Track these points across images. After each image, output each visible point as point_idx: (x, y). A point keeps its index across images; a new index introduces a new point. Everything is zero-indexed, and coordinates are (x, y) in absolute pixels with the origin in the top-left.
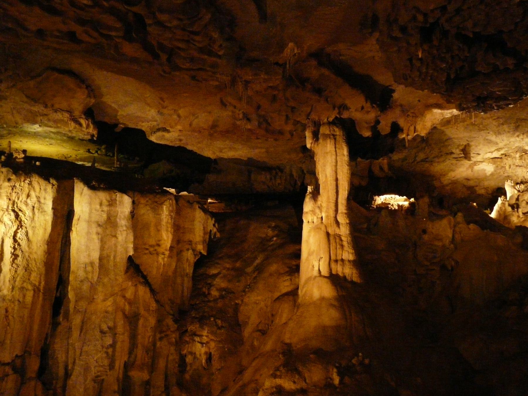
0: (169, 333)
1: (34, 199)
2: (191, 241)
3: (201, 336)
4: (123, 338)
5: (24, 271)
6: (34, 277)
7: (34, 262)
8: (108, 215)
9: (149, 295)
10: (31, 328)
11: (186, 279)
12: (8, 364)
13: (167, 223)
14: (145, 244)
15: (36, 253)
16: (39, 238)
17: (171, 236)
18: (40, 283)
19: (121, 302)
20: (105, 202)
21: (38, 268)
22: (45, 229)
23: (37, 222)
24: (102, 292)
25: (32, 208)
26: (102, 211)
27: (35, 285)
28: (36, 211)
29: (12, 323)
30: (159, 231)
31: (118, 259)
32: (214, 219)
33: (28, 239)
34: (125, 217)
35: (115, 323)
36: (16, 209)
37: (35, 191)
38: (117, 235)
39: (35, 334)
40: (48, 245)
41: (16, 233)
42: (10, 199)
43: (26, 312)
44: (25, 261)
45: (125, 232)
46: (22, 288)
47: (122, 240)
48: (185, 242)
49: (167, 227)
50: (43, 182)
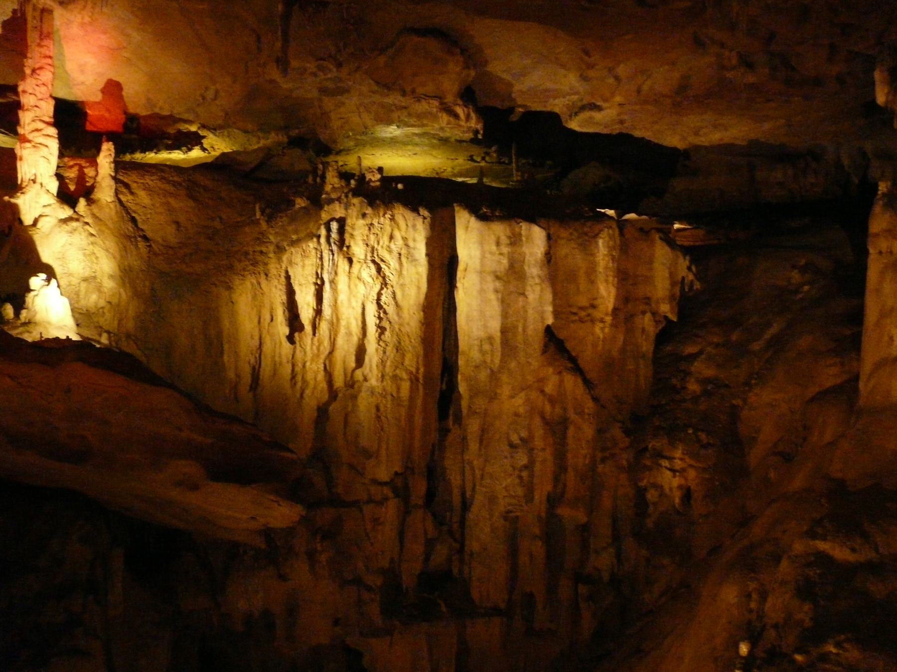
1: (400, 242)
3: (671, 459)
4: (545, 457)
5: (395, 351)
6: (409, 361)
12: (386, 484)
13: (606, 268)
16: (412, 302)
17: (613, 291)
18: (418, 369)
20: (504, 240)
21: (414, 347)
22: (419, 288)
26: (501, 254)
27: (411, 373)
28: (404, 260)
30: (592, 282)
32: (688, 258)
33: (397, 304)
34: (536, 261)
35: (530, 430)
36: (377, 260)
37: (399, 229)
38: (527, 293)
39: (417, 444)
40: (424, 311)
41: (379, 294)
42: (367, 245)
46: (395, 378)
50: (410, 215)
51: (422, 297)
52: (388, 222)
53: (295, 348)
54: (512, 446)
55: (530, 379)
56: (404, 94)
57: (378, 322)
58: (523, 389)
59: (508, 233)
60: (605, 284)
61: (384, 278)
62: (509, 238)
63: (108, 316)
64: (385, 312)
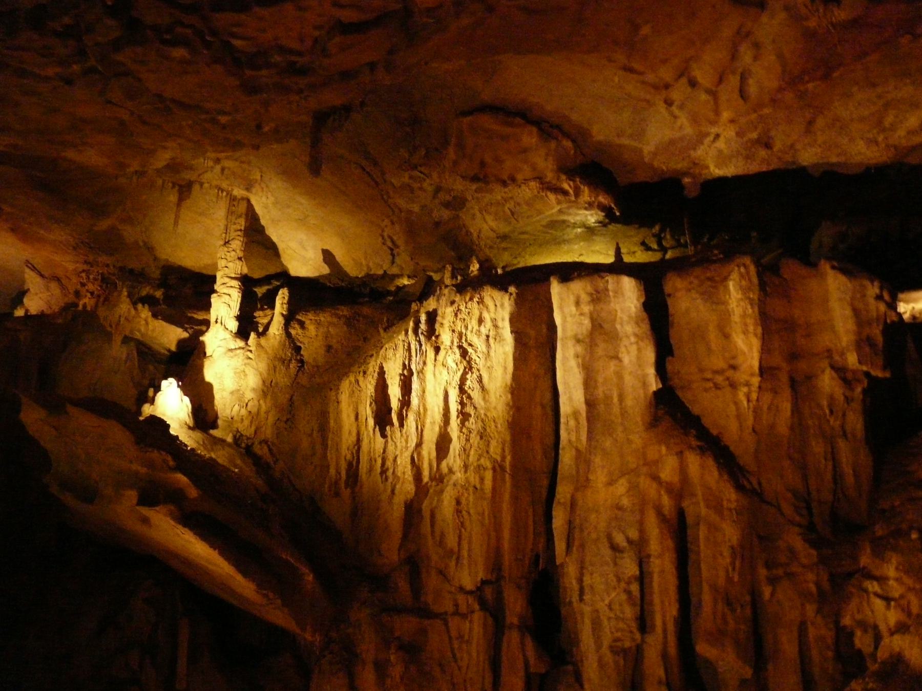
0: (795, 568)
1: (488, 324)
2: (829, 351)
3: (882, 580)
4: (662, 566)
5: (478, 437)
6: (495, 448)
7: (493, 424)
8: (592, 320)
9: (716, 473)
10: (499, 539)
11: (842, 444)
12: (470, 592)
13: (744, 316)
14: (701, 370)
15: (495, 408)
16: (498, 384)
17: (756, 343)
18: (503, 458)
19: (651, 489)
20: (585, 298)
21: (499, 433)
22: (505, 368)
23: (494, 360)
24: (603, 467)
25: (484, 337)
26: (581, 314)
27: (495, 461)
28: (491, 341)
29: (467, 524)
30: (727, 336)
31: (629, 402)
32: (876, 283)
33: (483, 388)
34: (630, 317)
35: (642, 531)
36: (465, 345)
37: (489, 312)
38: (620, 355)
39: (506, 545)
40: (512, 393)
41: (463, 380)
42: (453, 331)
43: (485, 505)
44: (479, 421)
45: (634, 347)
46: (480, 468)
47: (630, 361)
48: (818, 355)
49: (746, 325)
50: (497, 294)
51: (509, 377)
52: (475, 305)
53: (386, 442)
54: (614, 548)
55: (632, 462)
56: (504, 184)
57: (460, 407)
58: (623, 475)
59: (589, 289)
60: (742, 336)
61: (469, 362)
62: (591, 295)
63: (246, 423)
64: (469, 397)
